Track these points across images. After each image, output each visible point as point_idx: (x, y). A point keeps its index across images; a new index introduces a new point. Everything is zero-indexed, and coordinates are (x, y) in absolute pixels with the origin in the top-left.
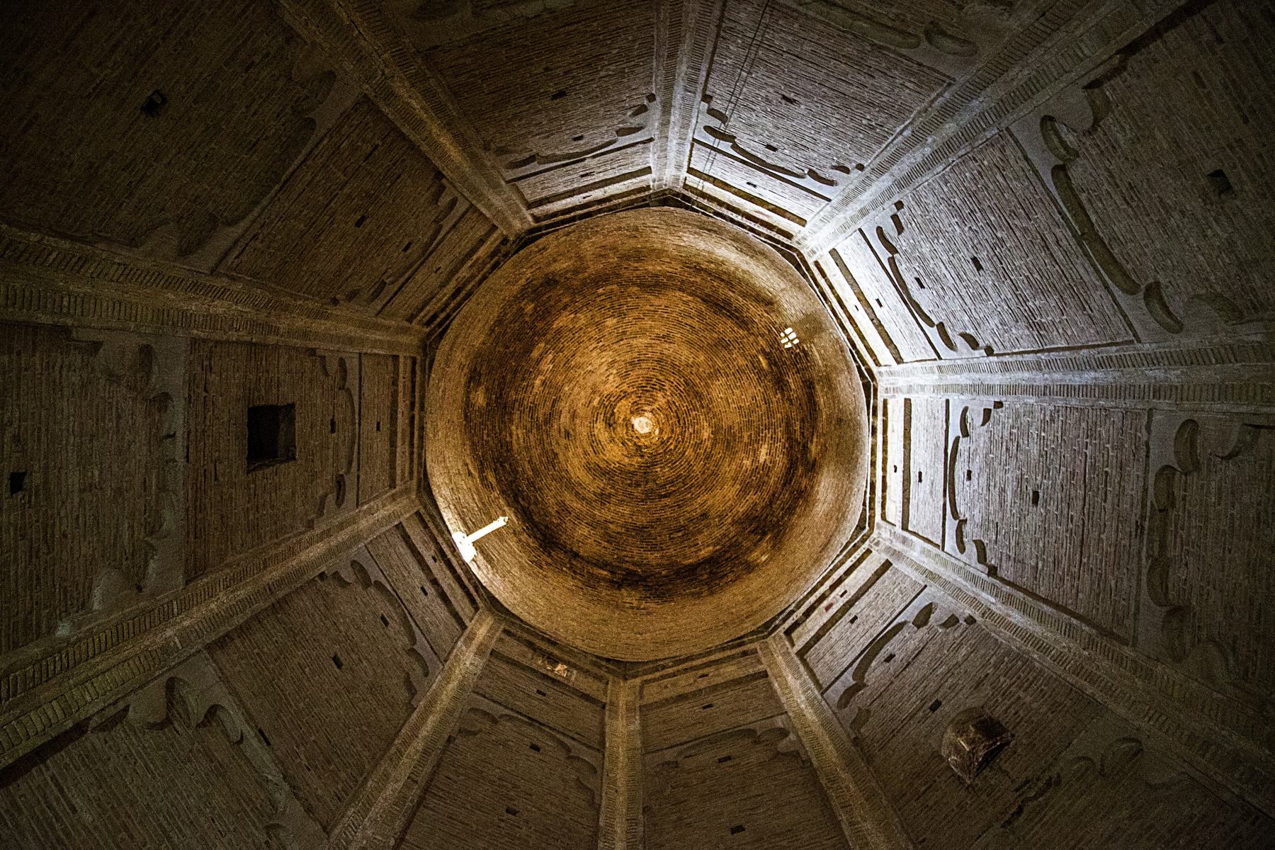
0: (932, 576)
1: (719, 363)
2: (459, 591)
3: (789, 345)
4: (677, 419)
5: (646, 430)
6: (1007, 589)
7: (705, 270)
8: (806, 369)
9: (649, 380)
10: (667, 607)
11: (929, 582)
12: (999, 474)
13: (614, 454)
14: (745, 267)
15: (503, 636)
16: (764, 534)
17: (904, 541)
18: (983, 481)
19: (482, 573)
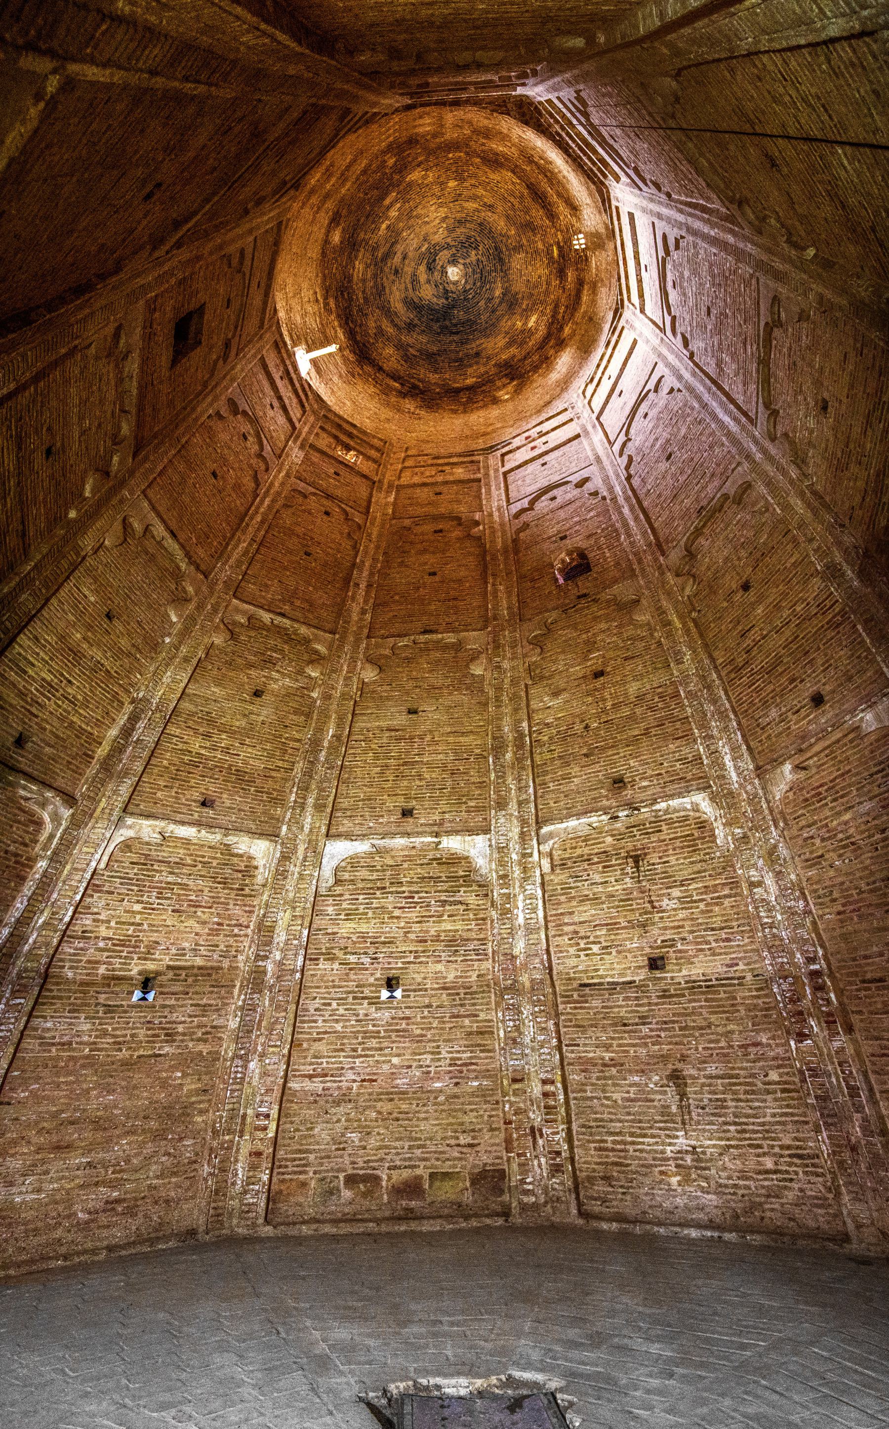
0: (598, 459)
1: (524, 241)
2: (295, 401)
3: (577, 247)
4: (480, 276)
5: (456, 278)
6: (630, 493)
7: (536, 164)
8: (583, 270)
9: (469, 238)
10: (431, 416)
11: (595, 463)
12: (660, 429)
13: (427, 293)
14: (565, 173)
15: (320, 431)
16: (512, 379)
17: (594, 427)
18: (651, 425)
19: (316, 383)
